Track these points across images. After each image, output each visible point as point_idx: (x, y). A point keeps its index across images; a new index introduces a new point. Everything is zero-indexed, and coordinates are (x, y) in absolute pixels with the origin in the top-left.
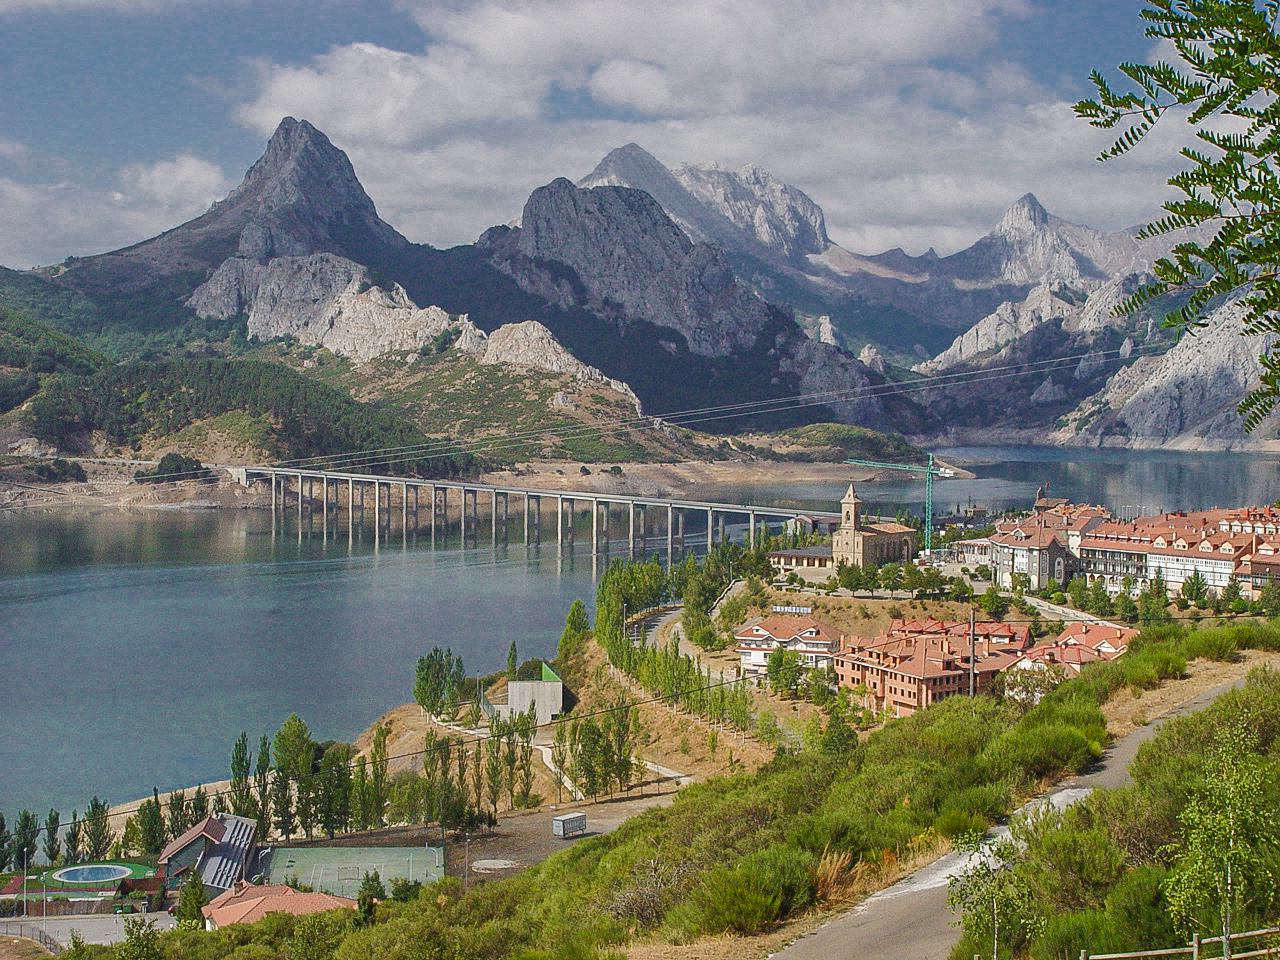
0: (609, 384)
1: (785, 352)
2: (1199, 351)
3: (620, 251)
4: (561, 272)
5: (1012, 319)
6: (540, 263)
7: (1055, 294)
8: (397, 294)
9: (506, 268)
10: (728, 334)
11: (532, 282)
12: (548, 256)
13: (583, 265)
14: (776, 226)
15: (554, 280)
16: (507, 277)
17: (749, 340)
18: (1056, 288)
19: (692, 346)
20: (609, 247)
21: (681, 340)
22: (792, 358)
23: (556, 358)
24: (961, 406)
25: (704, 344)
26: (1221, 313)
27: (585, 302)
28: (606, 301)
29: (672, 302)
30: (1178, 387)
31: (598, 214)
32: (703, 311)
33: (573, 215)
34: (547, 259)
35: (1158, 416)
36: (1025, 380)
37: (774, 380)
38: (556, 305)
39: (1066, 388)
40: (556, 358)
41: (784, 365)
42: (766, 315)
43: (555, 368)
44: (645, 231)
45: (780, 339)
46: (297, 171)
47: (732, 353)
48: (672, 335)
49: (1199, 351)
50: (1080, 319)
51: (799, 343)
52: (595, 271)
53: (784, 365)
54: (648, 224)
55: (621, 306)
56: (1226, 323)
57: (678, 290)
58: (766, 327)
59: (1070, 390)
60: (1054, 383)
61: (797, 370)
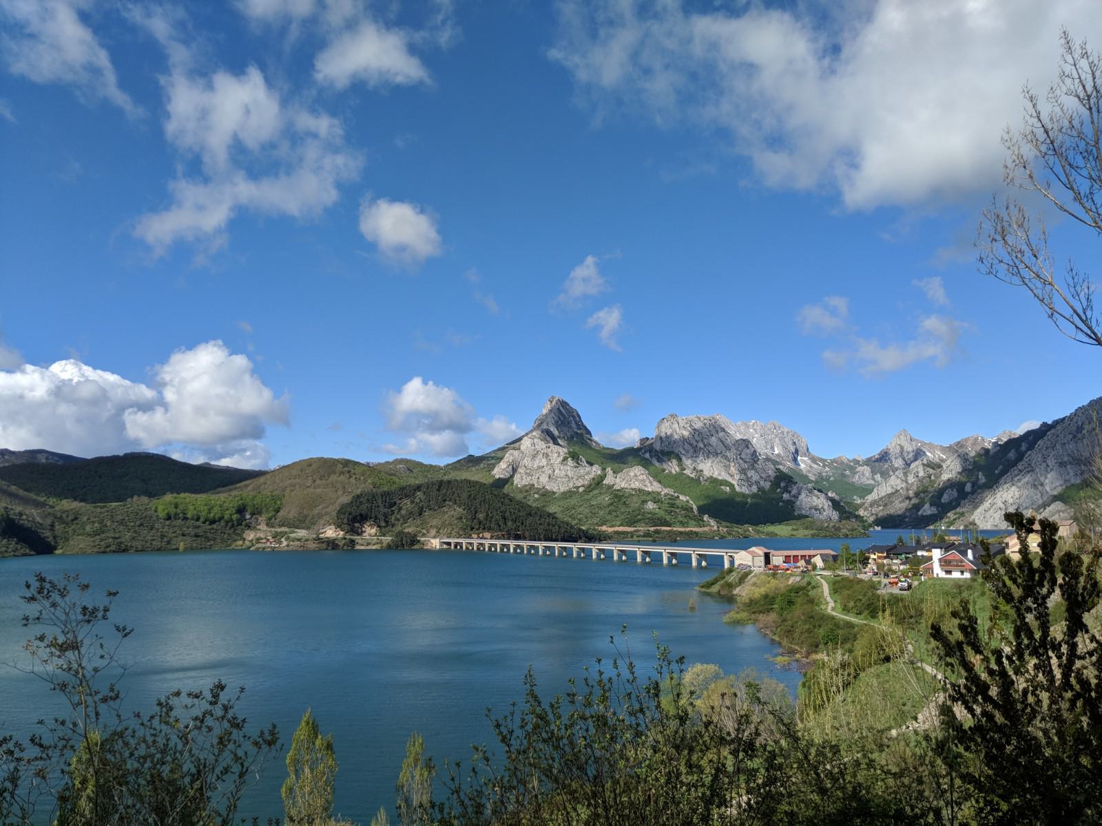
14: (785, 448)
21: (731, 486)
33: (678, 430)
41: (786, 496)
43: (650, 490)
56: (1027, 469)
61: (793, 499)
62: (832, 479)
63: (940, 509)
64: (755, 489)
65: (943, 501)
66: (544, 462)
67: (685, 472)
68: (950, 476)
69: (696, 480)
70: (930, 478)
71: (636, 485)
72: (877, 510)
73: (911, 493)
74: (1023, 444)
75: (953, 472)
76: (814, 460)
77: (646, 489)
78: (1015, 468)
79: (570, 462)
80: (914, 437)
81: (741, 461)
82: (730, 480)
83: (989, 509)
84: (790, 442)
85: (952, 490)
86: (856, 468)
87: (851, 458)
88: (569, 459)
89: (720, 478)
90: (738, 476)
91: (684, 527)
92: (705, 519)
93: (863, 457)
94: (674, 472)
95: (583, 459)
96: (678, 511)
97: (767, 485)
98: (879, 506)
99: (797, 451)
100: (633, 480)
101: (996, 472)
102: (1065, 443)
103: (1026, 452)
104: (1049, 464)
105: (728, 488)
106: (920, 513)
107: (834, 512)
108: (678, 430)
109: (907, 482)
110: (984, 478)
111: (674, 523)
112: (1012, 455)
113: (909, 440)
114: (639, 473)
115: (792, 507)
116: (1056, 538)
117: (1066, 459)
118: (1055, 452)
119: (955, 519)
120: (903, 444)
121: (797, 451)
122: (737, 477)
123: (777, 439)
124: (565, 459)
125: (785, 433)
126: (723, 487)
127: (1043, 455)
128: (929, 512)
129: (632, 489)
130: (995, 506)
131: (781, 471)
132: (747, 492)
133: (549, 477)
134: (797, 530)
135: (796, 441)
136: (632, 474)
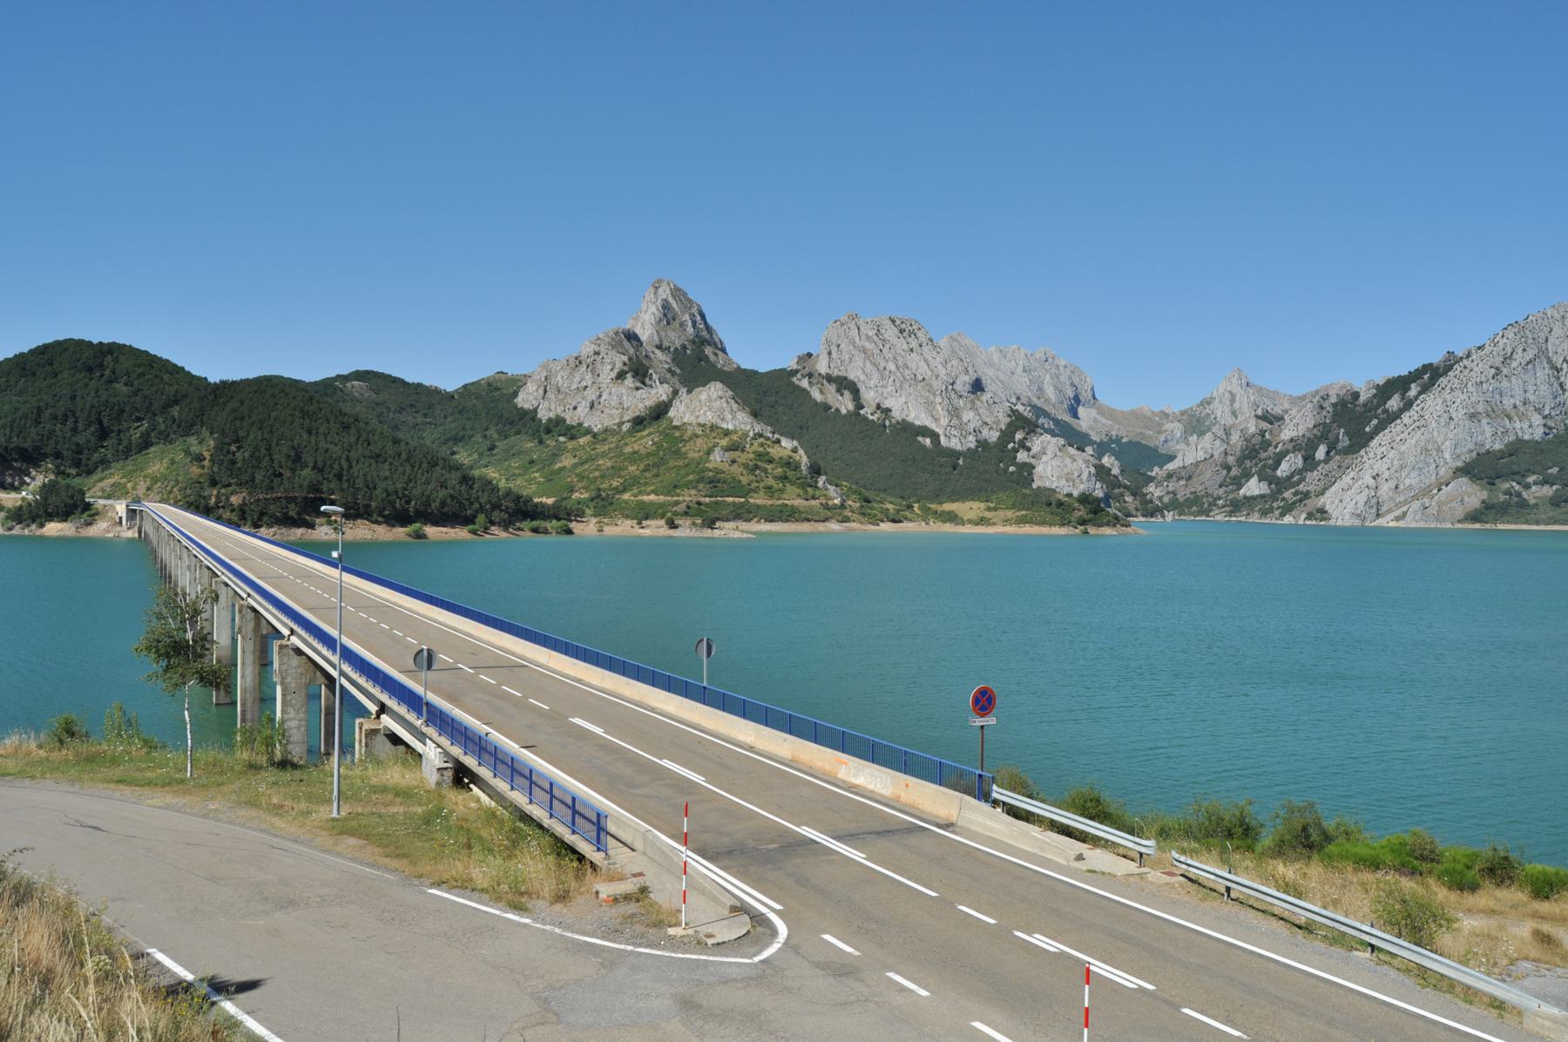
0: (778, 441)
1: (1023, 445)
2: (1392, 448)
3: (891, 366)
4: (845, 385)
5: (1224, 437)
6: (829, 378)
7: (1257, 417)
8: (651, 379)
9: (805, 383)
10: (975, 431)
11: (822, 392)
12: (836, 373)
13: (862, 379)
14: (1059, 390)
15: (839, 391)
16: (805, 390)
17: (993, 436)
18: (1259, 412)
19: (943, 440)
20: (883, 364)
21: (934, 436)
22: (1029, 450)
23: (731, 417)
24: (1181, 500)
25: (953, 440)
26: (1410, 417)
27: (862, 407)
28: (878, 407)
29: (929, 406)
30: (1374, 478)
31: (875, 338)
32: (954, 413)
33: (857, 339)
34: (835, 374)
35: (1356, 503)
36: (1235, 478)
37: (1012, 469)
38: (838, 410)
39: (1270, 484)
40: (731, 417)
41: (1022, 456)
42: (1009, 416)
43: (731, 427)
44: (912, 350)
45: (1019, 436)
46: (654, 315)
47: (977, 447)
48: (925, 431)
49: (1392, 448)
50: (1281, 431)
51: (1035, 438)
52: (872, 384)
53: (1022, 456)
54: (914, 344)
55: (889, 410)
56: (1417, 424)
57: (934, 395)
58: (1009, 425)
59: (1273, 486)
60: (1260, 481)
61: (1032, 460)
62: (1124, 440)
63: (1273, 486)
64: (971, 442)
65: (1279, 473)
66: (588, 380)
67: (862, 412)
68: (1294, 434)
69: (879, 425)
70: (1263, 436)
71: (708, 417)
72: (1177, 485)
73: (1231, 460)
74: (1413, 386)
75: (1300, 427)
76: (1102, 411)
77: (724, 426)
78: (1398, 421)
79: (629, 381)
80: (1252, 381)
81: (953, 396)
82: (933, 426)
83: (1350, 488)
84: (1068, 383)
85: (1296, 457)
86: (1163, 425)
87: (1157, 410)
88: (629, 375)
89: (918, 423)
90: (947, 421)
91: (771, 497)
92: (820, 484)
93: (1176, 407)
94: (844, 411)
95: (654, 376)
96: (769, 467)
97: (993, 436)
98: (1180, 479)
99: (1077, 399)
100: (705, 408)
101: (1367, 429)
102: (1482, 383)
103: (1416, 398)
104: (1454, 416)
105: (928, 441)
106: (1242, 492)
107: (1098, 485)
108: (857, 339)
109: (1228, 444)
110: (1346, 438)
111: (756, 490)
112: (1394, 403)
113: (1244, 385)
114: (715, 396)
115: (1030, 474)
116: (286, 727)
117: (1481, 408)
118: (1465, 396)
119: (1294, 503)
120: (1234, 392)
121: (1077, 399)
122: (944, 421)
123: (1048, 377)
124: (621, 376)
125: (1061, 368)
126: (920, 439)
127: (1445, 401)
128: (1256, 492)
129: (700, 425)
130: (1360, 482)
131: (1020, 414)
132: (959, 448)
133: (592, 406)
134: (995, 509)
135: (1076, 381)
136: (704, 396)
